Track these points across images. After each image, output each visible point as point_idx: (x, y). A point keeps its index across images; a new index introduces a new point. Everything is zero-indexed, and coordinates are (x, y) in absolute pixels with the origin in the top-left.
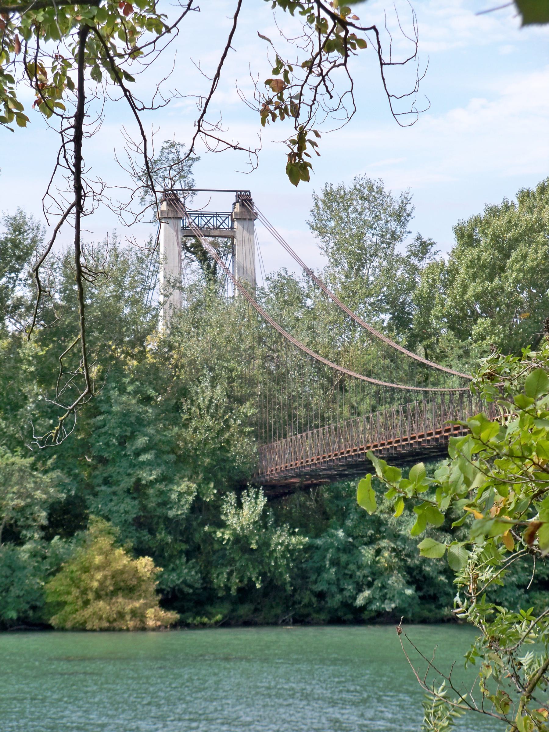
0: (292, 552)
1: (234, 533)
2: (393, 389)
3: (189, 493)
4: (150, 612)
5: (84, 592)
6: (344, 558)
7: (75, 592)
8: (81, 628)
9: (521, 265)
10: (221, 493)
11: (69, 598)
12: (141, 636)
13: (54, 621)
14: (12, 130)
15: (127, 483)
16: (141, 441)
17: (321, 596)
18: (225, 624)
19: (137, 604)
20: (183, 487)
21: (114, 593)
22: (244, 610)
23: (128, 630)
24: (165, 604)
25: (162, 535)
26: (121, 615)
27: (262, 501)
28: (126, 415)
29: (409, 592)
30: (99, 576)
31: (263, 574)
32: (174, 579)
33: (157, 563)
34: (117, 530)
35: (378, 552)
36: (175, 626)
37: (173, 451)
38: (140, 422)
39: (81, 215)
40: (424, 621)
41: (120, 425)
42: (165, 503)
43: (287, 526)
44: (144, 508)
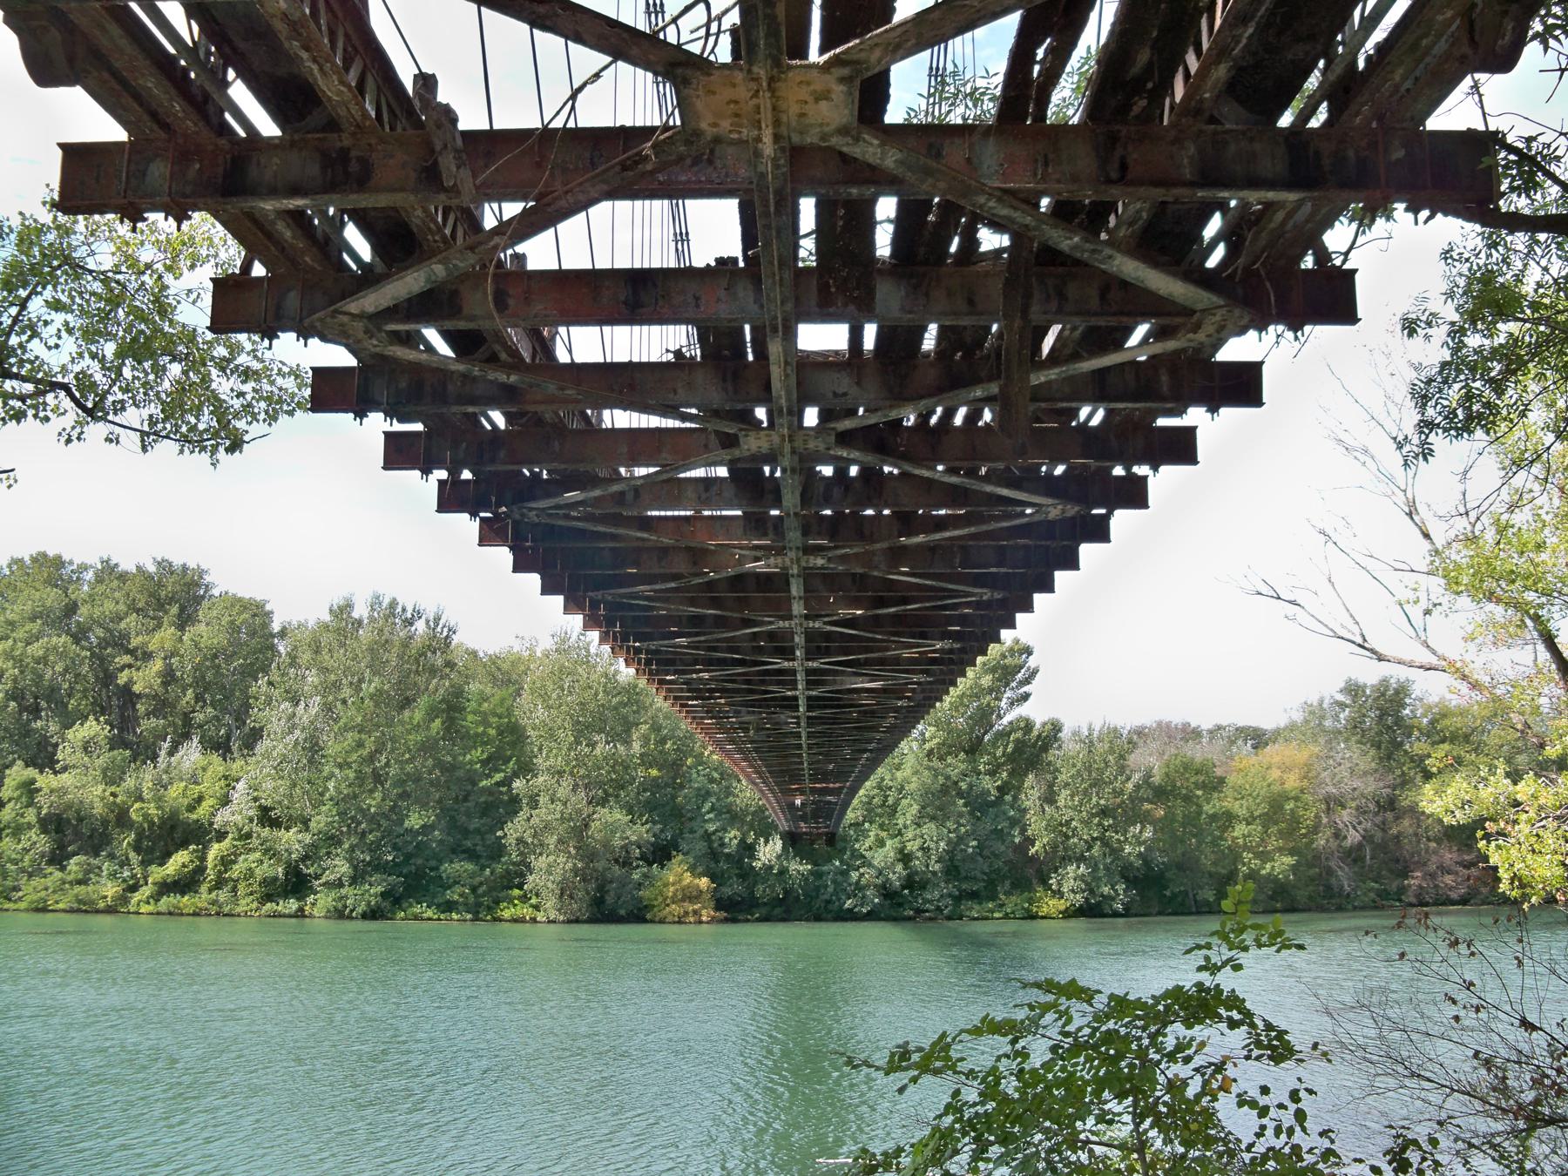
4: (704, 912)
5: (665, 899)
6: (840, 878)
11: (656, 903)
13: (648, 916)
16: (707, 806)
18: (759, 920)
21: (683, 900)
22: (778, 911)
23: (129, 913)
29: (876, 900)
30: (672, 889)
36: (726, 920)
37: (728, 812)
38: (708, 794)
42: (723, 845)
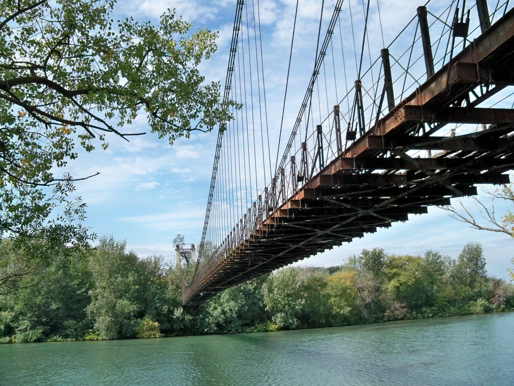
0: (190, 320)
1: (177, 317)
2: (258, 209)
3: (166, 308)
4: (157, 334)
6: (202, 321)
8: (142, 338)
10: (174, 308)
11: (140, 332)
13: (138, 336)
14: (98, 173)
15: (154, 307)
17: (198, 329)
19: (154, 332)
20: (165, 307)
22: (181, 333)
24: (161, 332)
25: (163, 318)
26: (151, 335)
27: (182, 310)
28: (153, 292)
29: (216, 328)
30: (146, 326)
32: (164, 327)
33: (159, 323)
34: (151, 316)
35: (209, 319)
39: (50, 58)
41: (152, 294)
42: (162, 311)
43: (188, 315)
44: (158, 312)
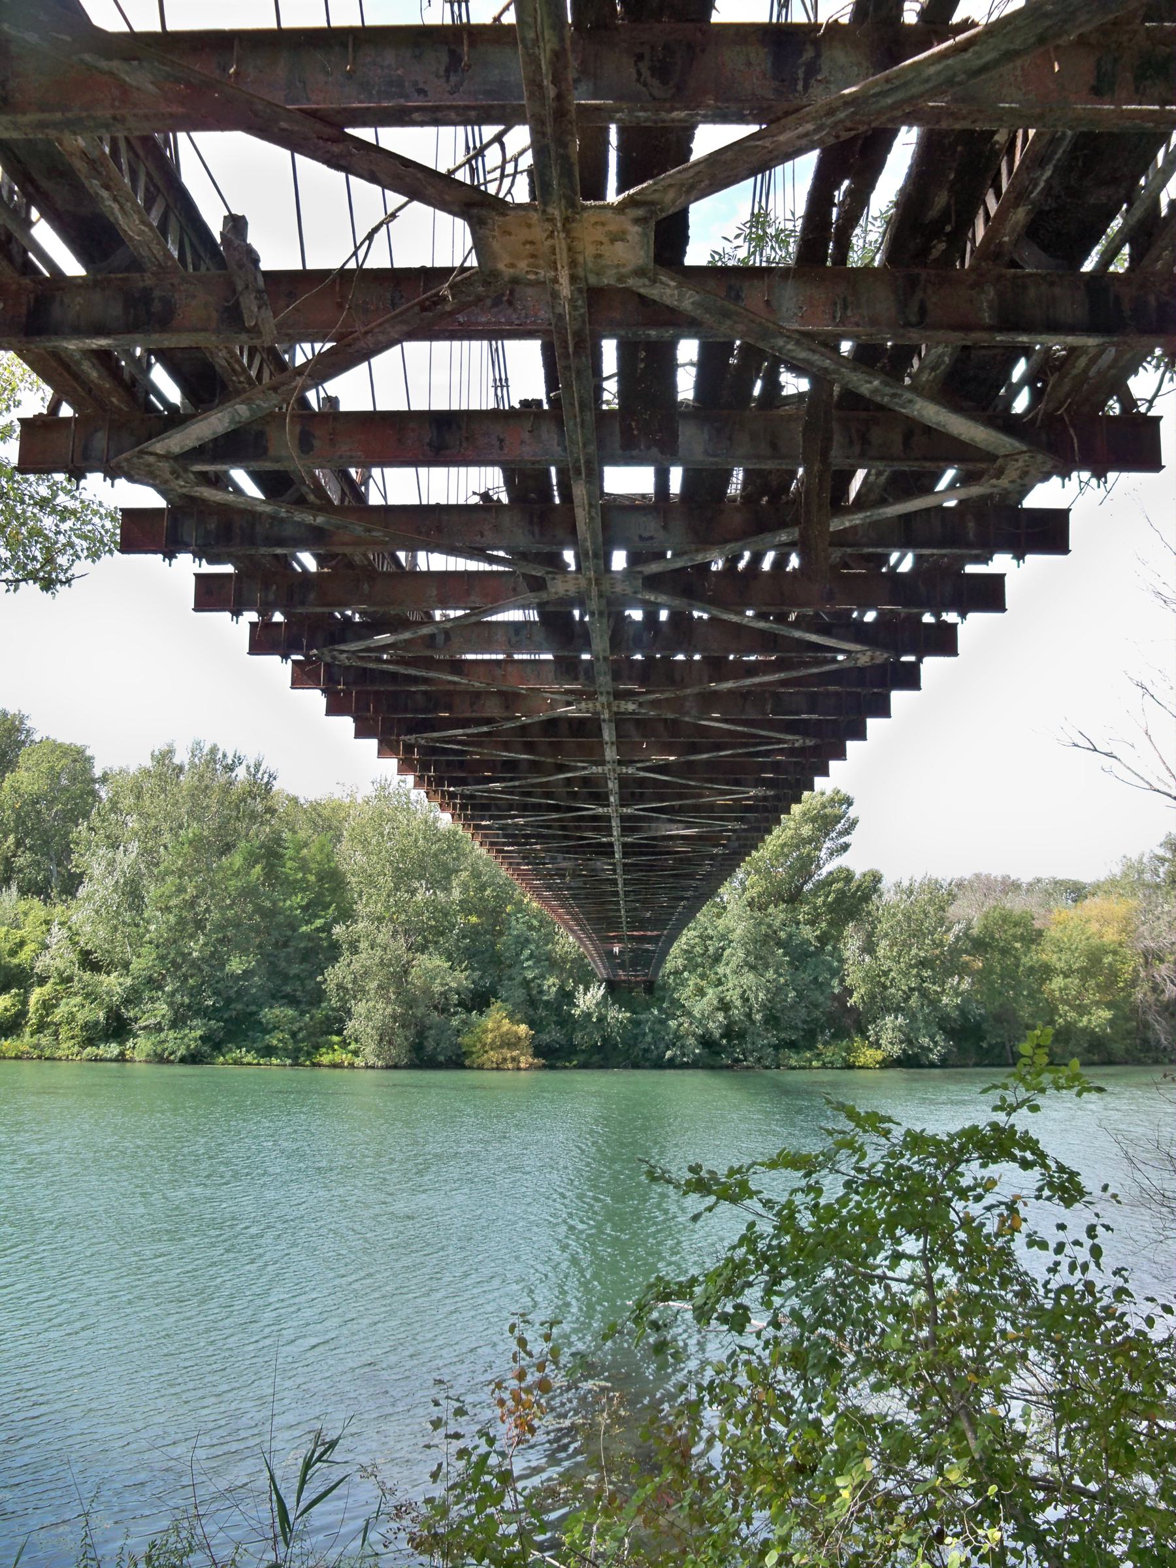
4: (522, 1059)
7: (479, 1046)
9: (601, 596)
12: (516, 1073)
13: (467, 1062)
15: (519, 979)
16: (527, 952)
18: (976, 1065)
20: (551, 981)
27: (602, 991)
28: (518, 936)
31: (603, 1037)
32: (545, 1038)
36: (544, 1067)
38: (528, 940)
40: (712, 1068)
42: (541, 992)
